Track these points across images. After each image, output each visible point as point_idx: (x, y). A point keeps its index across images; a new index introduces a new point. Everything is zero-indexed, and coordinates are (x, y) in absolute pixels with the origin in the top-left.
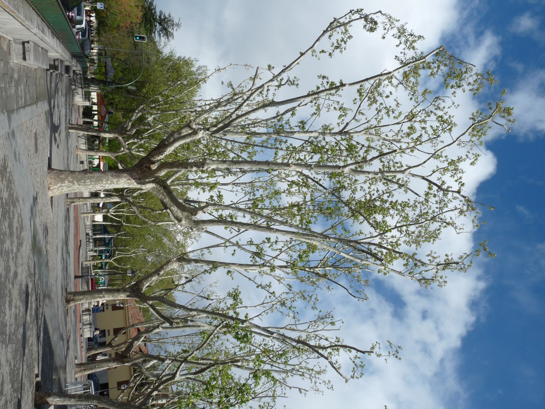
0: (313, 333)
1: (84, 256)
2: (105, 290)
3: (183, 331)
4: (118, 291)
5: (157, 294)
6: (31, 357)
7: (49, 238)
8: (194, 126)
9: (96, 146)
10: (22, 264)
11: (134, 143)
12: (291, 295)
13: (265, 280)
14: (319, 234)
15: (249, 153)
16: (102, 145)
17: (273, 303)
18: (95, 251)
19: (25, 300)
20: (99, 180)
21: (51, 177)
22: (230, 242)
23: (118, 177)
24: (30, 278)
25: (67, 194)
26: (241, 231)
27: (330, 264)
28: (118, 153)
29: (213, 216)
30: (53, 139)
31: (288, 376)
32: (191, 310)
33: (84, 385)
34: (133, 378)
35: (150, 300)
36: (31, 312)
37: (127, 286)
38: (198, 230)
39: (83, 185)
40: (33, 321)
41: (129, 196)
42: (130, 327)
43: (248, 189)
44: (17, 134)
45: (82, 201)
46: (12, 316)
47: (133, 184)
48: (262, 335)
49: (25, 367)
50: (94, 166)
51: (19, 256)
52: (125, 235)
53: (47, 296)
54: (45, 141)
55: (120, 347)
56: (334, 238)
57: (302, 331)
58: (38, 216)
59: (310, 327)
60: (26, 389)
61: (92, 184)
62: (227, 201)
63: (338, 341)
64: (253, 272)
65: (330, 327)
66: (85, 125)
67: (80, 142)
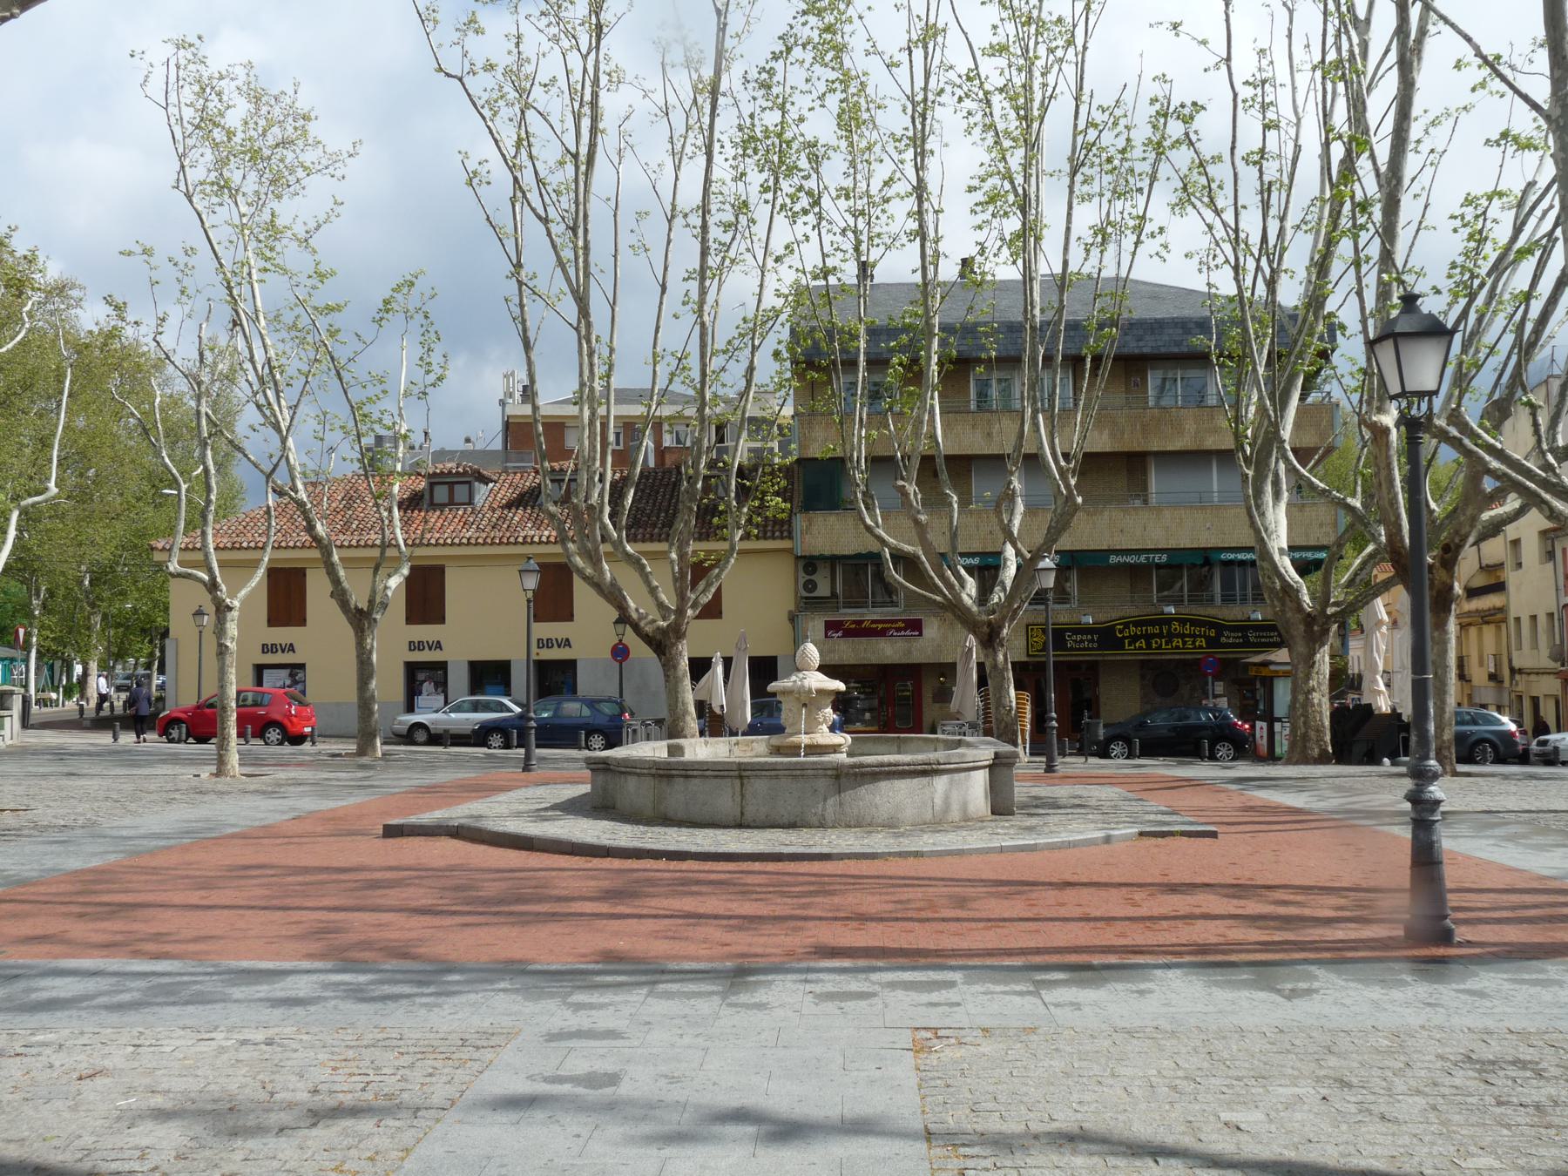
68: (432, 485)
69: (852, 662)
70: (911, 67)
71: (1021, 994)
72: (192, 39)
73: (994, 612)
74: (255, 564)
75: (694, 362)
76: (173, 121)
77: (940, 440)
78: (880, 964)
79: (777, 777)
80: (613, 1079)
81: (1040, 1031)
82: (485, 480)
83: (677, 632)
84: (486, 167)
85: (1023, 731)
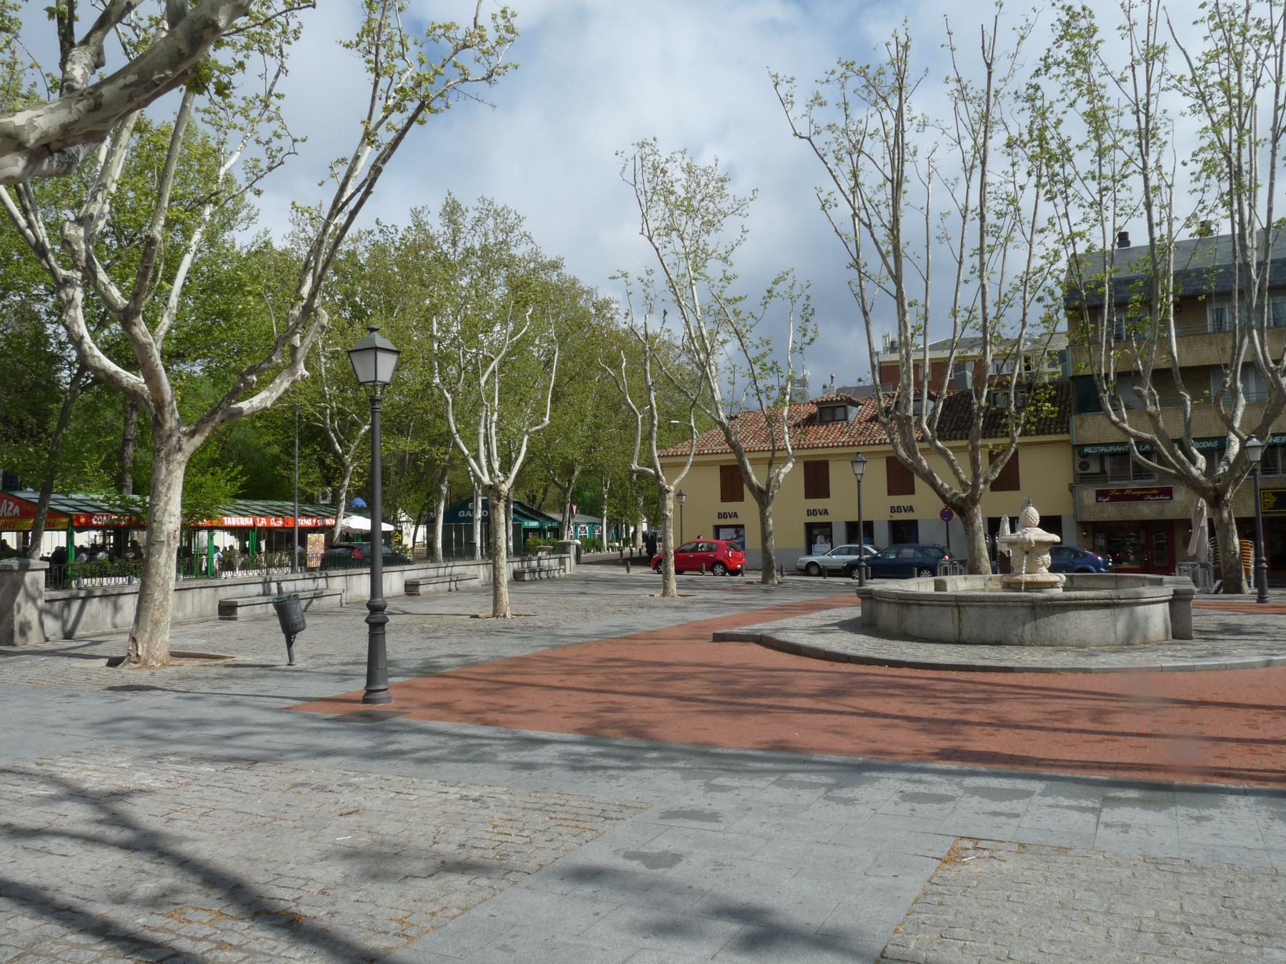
28: (160, 405)
68: (821, 409)
69: (1118, 519)
70: (1135, 79)
71: (1082, 810)
72: (650, 141)
73: (1219, 481)
74: (684, 465)
75: (979, 313)
76: (639, 193)
77: (1176, 355)
78: (983, 768)
79: (985, 607)
80: (672, 859)
81: (1072, 852)
82: (856, 404)
83: (973, 500)
84: (834, 196)
85: (1247, 571)
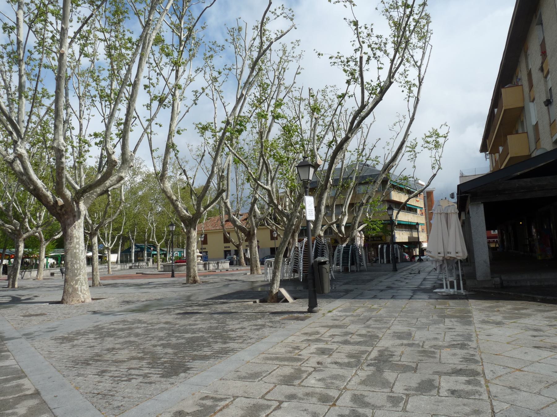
0: (247, 52)
1: (153, 270)
2: (187, 250)
3: (232, 180)
4: (189, 238)
5: (195, 203)
6: (239, 307)
7: (135, 299)
8: (12, 157)
9: (33, 262)
10: (158, 319)
11: (30, 222)
12: (208, 69)
13: (189, 95)
14: (144, 31)
15: (43, 96)
16: (32, 254)
17: (213, 89)
18: (148, 260)
19: (191, 315)
20: (75, 256)
21: (71, 300)
22: (147, 128)
23: (72, 237)
24: (171, 312)
25: (90, 286)
26: (136, 116)
27: (178, 21)
28: (41, 238)
29: (117, 143)
30: (28, 301)
31: (284, 84)
32: (213, 172)
33: (268, 266)
34: (269, 227)
35: (200, 209)
36: (202, 309)
37: (185, 230)
38: (132, 160)
39: (80, 271)
40: (209, 307)
41: (92, 228)
42: (223, 229)
43: (88, 102)
44: (27, 331)
45: (96, 272)
46: (203, 323)
47: (80, 223)
48: (243, 105)
49: (246, 311)
50: (55, 263)
51: (151, 322)
52: (133, 232)
53: (188, 298)
54: (31, 308)
55: (241, 238)
56: (150, 13)
57: (244, 63)
58: (112, 310)
59: (241, 54)
60: (264, 309)
61: (80, 262)
62: (101, 128)
63: (257, 27)
64: (180, 106)
65: (243, 33)
66: (9, 272)
67: (29, 277)
